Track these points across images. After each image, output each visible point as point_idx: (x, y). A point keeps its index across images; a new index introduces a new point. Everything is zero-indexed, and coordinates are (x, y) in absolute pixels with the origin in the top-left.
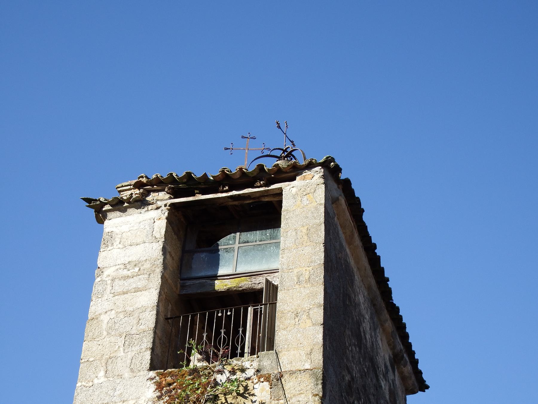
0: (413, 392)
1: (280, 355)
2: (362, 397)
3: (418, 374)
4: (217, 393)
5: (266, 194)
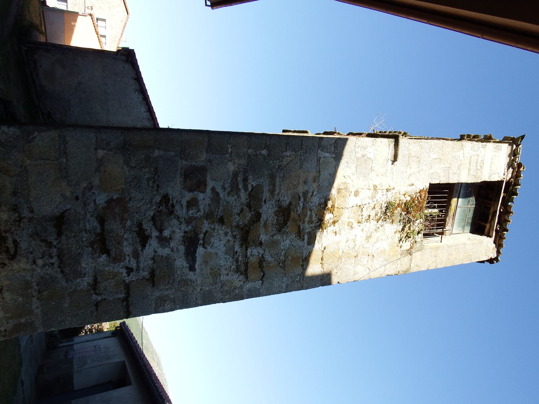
1: (420, 252)
5: (491, 228)
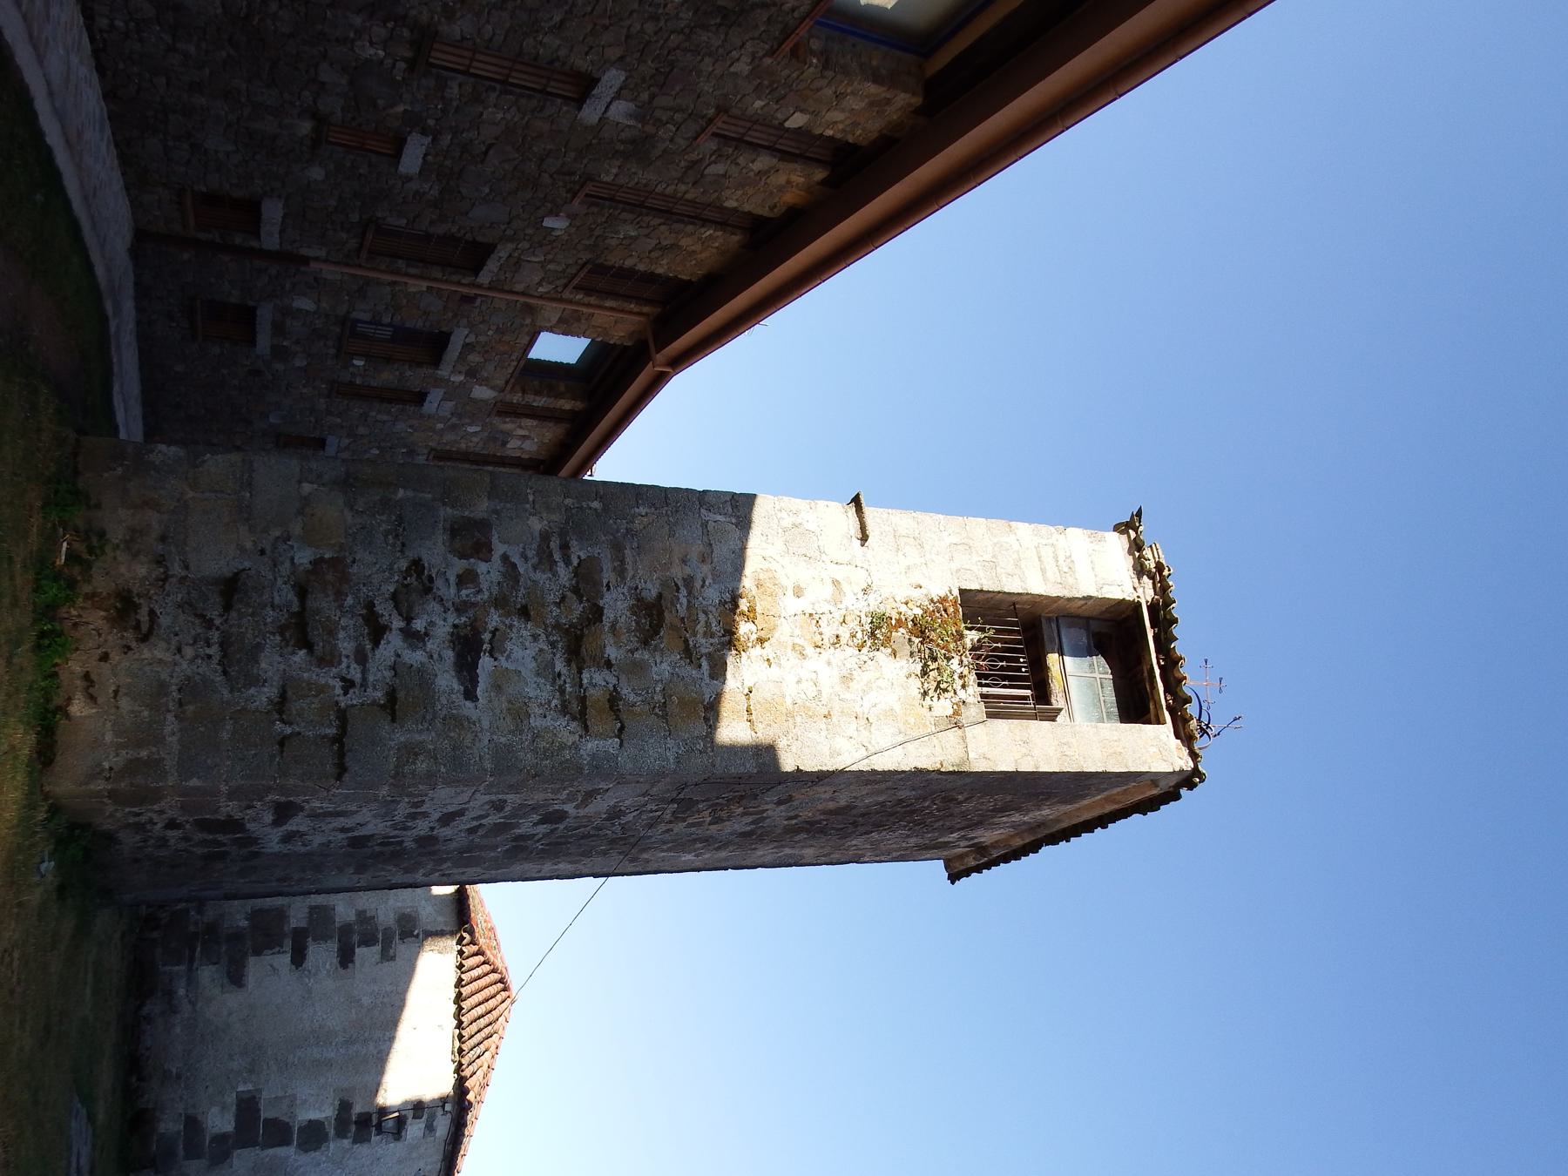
3: (967, 872)
4: (940, 661)
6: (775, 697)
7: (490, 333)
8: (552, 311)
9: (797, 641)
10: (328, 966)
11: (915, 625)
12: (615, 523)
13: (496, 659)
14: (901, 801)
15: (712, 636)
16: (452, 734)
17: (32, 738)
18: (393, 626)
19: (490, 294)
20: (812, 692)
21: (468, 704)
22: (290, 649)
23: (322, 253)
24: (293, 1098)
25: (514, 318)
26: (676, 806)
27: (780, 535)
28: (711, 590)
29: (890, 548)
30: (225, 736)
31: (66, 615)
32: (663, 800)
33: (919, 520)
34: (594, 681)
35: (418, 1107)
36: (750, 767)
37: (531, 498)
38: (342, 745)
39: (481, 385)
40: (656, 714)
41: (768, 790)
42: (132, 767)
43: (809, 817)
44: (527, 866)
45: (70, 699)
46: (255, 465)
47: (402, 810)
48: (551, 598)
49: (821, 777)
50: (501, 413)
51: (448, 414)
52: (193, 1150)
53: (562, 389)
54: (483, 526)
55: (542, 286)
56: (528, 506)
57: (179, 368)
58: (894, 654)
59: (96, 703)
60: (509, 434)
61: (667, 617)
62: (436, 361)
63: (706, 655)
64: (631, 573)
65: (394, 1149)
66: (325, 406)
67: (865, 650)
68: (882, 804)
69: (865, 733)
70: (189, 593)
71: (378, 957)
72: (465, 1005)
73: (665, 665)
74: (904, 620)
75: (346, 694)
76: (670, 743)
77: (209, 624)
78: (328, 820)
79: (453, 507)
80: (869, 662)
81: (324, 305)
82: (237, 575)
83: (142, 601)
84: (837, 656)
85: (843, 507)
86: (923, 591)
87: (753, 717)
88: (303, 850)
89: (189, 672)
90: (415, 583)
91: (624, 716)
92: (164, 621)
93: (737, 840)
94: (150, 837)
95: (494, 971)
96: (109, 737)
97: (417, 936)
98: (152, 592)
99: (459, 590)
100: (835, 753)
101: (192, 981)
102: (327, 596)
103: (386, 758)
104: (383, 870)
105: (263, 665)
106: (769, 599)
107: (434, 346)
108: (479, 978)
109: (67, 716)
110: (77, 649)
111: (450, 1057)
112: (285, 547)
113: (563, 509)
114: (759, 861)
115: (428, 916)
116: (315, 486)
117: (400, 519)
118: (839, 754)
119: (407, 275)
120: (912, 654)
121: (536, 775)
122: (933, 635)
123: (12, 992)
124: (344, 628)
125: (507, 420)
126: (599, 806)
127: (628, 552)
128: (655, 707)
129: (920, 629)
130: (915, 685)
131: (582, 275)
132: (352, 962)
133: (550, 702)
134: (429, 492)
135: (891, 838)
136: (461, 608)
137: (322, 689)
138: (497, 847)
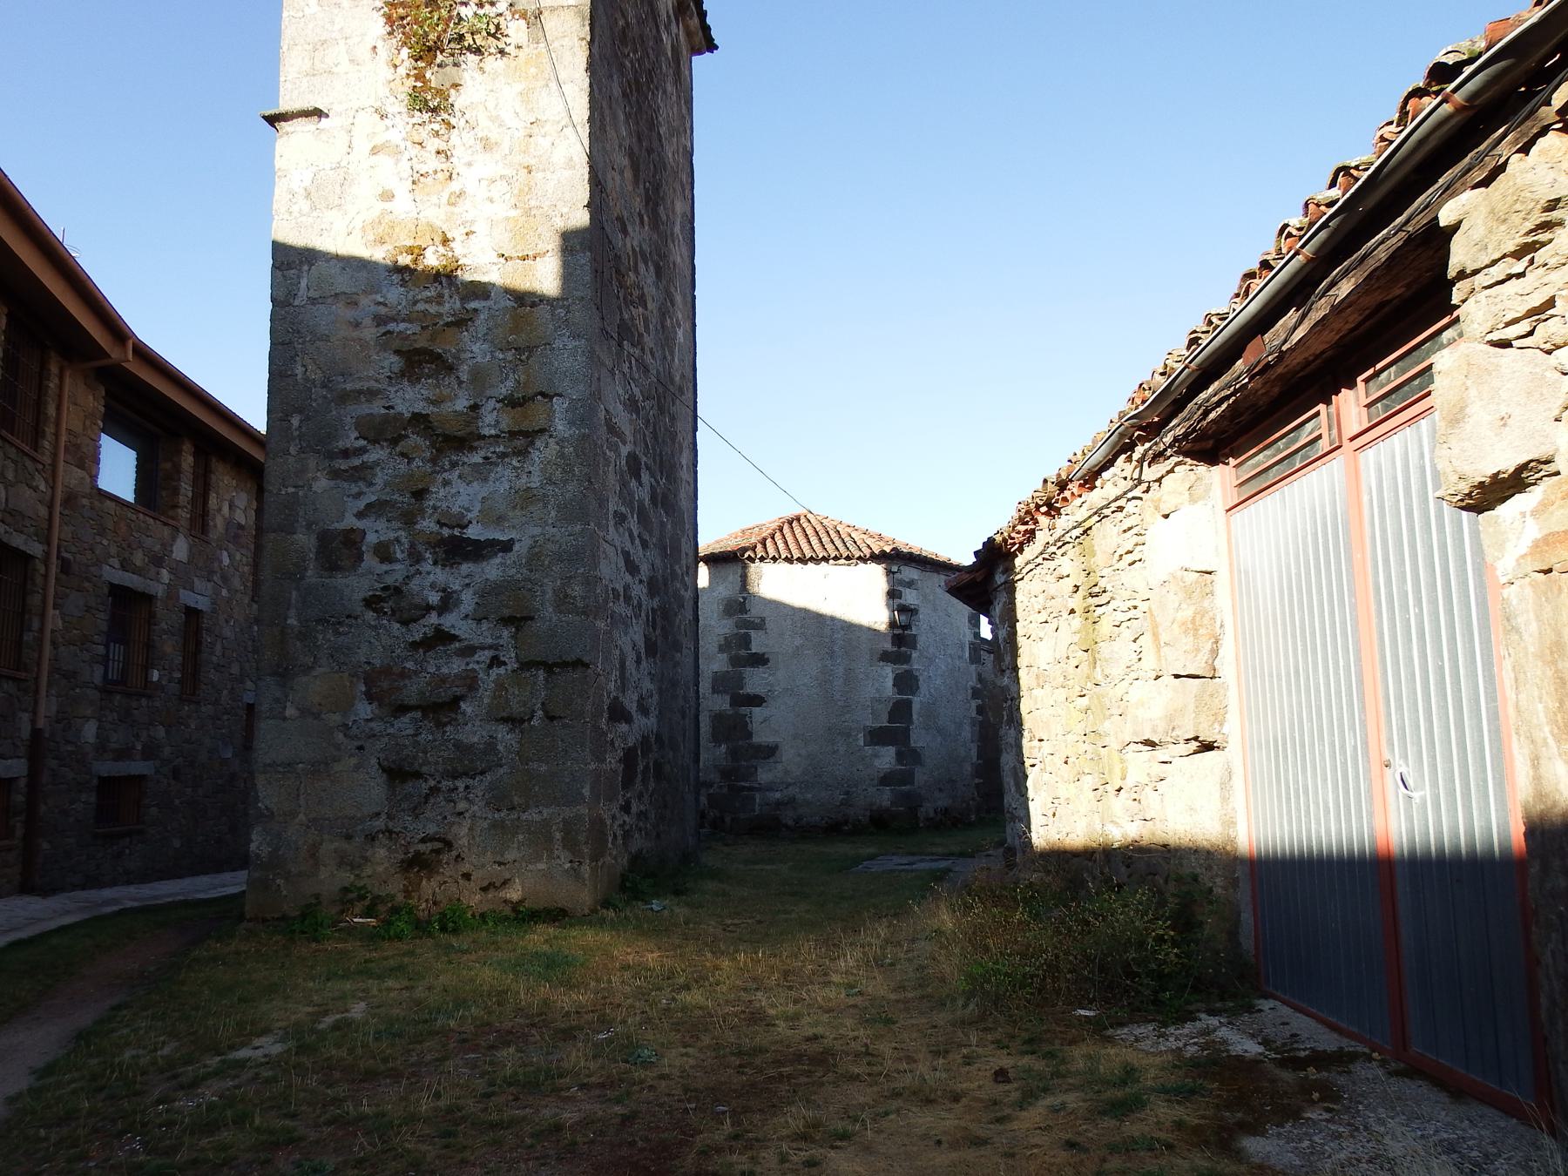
0: (700, 53)
2: (639, 50)
3: (706, 29)
4: (463, 31)
6: (508, 228)
7: (105, 542)
8: (70, 476)
9: (444, 200)
10: (766, 675)
11: (421, 58)
12: (316, 400)
13: (470, 522)
14: (624, 94)
15: (441, 296)
16: (546, 562)
17: (541, 928)
18: (436, 623)
19: (55, 542)
20: (501, 186)
21: (516, 547)
22: (459, 717)
23: (25, 717)
24: (874, 700)
25: (83, 517)
26: (625, 342)
27: (320, 215)
28: (389, 296)
29: (329, 82)
30: (544, 768)
31: (426, 912)
32: (619, 355)
33: (292, 43)
34: (493, 423)
35: (892, 594)
36: (584, 259)
37: (291, 490)
38: (556, 665)
39: (172, 551)
40: (528, 358)
41: (610, 242)
42: (570, 843)
43: (642, 201)
44: (683, 495)
45: (505, 901)
46: (268, 761)
47: (621, 608)
48: (403, 467)
49: (597, 182)
50: (204, 529)
51: (210, 585)
52: (907, 778)
53: (168, 466)
54: (325, 538)
55: (37, 487)
56: (301, 493)
57: (177, 843)
58: (456, 86)
59: (509, 880)
60: (229, 523)
61: (422, 345)
62: (148, 598)
63: (462, 304)
64: (373, 384)
65: (924, 615)
66: (210, 706)
67: (453, 121)
68: (628, 116)
69: (548, 128)
70: (403, 810)
71: (761, 633)
72: (808, 554)
73: (475, 348)
74: (416, 72)
75: (505, 663)
76: (558, 344)
77: (434, 790)
78: (628, 675)
79: (306, 569)
80: (467, 117)
81: (89, 712)
82: (384, 770)
83: (412, 850)
84: (460, 156)
85: (281, 136)
86: (380, 44)
87: (530, 253)
88: (656, 697)
89: (482, 804)
90: (390, 603)
91: (531, 392)
92: (432, 829)
93: (664, 282)
94: (636, 826)
95: (781, 529)
96: (542, 866)
97: (745, 599)
98: (403, 842)
99: (397, 560)
100: (570, 162)
101: (770, 787)
102: (405, 685)
103: (568, 624)
104: (679, 627)
105: (476, 740)
106: (397, 230)
107: (127, 603)
108: (786, 543)
109: (521, 902)
110: (459, 900)
111: (852, 567)
112: (355, 727)
113: (303, 455)
114: (688, 261)
115: (727, 590)
116: (288, 704)
117: (319, 621)
118: (571, 159)
119: (41, 630)
120: (456, 65)
121: (589, 481)
122: (433, 36)
123: (760, 922)
124: (438, 668)
125: (211, 523)
126: (623, 419)
127: (349, 386)
128: (520, 359)
129: (426, 52)
130: (492, 63)
131: (18, 442)
132: (764, 654)
133: (515, 468)
134: (290, 593)
135: (666, 113)
136: (415, 557)
137: (500, 685)
138: (662, 522)
